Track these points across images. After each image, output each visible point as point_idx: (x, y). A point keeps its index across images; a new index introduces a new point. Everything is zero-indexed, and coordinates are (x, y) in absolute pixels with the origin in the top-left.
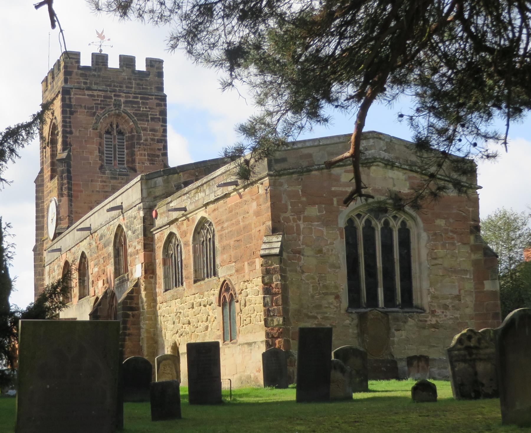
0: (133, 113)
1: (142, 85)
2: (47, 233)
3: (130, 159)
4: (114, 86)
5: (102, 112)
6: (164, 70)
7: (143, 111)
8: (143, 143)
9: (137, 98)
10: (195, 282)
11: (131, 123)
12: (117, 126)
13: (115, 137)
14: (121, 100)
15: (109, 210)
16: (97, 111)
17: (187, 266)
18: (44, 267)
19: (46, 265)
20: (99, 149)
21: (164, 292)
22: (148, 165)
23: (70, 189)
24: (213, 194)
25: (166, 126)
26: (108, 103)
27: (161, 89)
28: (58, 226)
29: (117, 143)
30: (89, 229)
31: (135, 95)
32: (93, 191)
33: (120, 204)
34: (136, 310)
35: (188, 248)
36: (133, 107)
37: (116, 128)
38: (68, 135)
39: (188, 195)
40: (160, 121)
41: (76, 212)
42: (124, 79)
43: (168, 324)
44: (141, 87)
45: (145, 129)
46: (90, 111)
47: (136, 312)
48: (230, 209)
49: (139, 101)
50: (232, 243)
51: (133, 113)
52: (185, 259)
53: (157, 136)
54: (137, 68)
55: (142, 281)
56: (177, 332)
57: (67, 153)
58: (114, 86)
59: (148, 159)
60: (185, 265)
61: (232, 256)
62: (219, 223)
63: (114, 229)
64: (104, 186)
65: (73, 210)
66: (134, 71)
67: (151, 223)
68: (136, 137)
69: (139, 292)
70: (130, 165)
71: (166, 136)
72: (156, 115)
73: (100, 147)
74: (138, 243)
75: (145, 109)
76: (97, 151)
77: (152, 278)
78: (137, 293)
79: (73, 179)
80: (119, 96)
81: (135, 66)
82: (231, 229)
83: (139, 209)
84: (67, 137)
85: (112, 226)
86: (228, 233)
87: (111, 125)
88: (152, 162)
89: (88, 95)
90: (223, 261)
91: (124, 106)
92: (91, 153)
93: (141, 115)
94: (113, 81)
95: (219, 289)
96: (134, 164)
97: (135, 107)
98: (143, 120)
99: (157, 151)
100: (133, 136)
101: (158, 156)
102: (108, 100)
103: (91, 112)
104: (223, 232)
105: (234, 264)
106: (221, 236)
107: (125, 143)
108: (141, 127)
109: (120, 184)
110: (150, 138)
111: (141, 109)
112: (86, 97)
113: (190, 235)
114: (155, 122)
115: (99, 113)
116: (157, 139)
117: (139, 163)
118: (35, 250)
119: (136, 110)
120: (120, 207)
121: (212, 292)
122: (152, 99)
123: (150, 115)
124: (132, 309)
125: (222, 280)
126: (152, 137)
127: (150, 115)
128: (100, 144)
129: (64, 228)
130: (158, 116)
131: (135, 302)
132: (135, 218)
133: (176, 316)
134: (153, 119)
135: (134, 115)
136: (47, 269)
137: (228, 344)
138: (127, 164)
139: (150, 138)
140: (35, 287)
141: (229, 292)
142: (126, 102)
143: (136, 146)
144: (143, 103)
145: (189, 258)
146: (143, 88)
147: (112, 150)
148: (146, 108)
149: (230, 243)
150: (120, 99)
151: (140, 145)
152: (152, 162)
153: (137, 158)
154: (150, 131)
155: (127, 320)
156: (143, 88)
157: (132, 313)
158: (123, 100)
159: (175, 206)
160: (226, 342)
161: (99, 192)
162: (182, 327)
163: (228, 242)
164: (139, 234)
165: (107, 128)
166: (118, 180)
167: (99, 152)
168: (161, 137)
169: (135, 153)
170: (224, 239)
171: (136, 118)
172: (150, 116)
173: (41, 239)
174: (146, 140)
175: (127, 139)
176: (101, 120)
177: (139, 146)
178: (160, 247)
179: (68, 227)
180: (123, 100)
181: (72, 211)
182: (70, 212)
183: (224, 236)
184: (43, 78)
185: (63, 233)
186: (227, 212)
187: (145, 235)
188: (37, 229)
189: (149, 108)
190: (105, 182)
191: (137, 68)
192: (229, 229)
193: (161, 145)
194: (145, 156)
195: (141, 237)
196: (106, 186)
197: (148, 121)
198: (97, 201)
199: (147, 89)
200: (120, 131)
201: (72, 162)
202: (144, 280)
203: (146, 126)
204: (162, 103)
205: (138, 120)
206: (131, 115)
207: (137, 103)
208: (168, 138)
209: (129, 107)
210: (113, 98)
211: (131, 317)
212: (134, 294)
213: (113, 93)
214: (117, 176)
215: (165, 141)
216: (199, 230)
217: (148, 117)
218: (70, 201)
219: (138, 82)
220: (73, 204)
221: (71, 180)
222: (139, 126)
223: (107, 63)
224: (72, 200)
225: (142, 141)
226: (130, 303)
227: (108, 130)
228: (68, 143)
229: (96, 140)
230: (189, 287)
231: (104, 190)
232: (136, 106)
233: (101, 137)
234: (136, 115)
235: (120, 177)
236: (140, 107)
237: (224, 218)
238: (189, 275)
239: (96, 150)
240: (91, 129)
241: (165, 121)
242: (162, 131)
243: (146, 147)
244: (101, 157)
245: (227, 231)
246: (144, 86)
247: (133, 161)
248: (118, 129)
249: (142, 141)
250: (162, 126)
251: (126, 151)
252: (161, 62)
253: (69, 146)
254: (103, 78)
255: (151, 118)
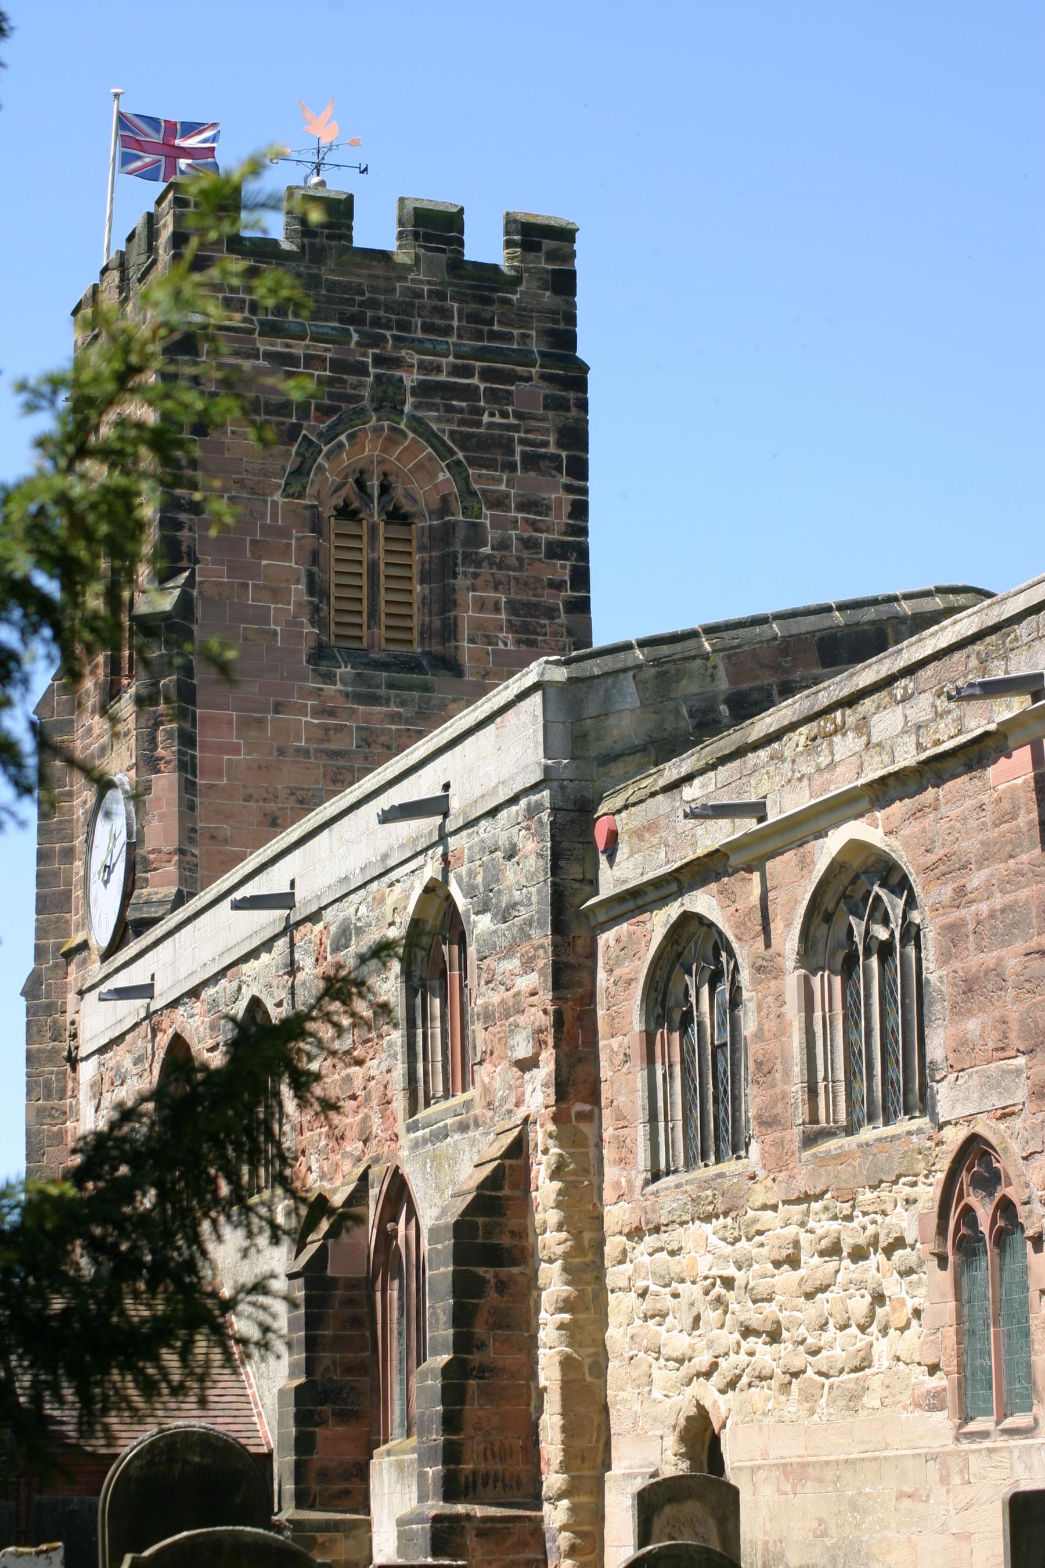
0: (452, 434)
1: (491, 323)
2: (86, 922)
3: (437, 623)
4: (376, 322)
5: (323, 426)
6: (580, 265)
7: (491, 425)
8: (488, 557)
9: (468, 372)
10: (810, 1140)
11: (444, 476)
12: (385, 489)
13: (373, 529)
14: (401, 379)
15: (390, 816)
16: (305, 423)
17: (765, 1068)
18: (73, 1061)
19: (83, 1053)
20: (311, 575)
21: (647, 1183)
22: (511, 647)
23: (187, 740)
24: (911, 740)
25: (585, 491)
26: (350, 391)
27: (569, 340)
28: (136, 892)
29: (382, 554)
30: (284, 900)
31: (459, 361)
32: (281, 752)
33: (439, 793)
34: (514, 1263)
35: (773, 984)
36: (450, 409)
37: (381, 495)
38: (183, 517)
39: (776, 745)
40: (559, 469)
41: (213, 837)
42: (419, 295)
43: (663, 1329)
44: (486, 328)
45: (499, 502)
46: (280, 419)
47: (515, 1270)
48: (1006, 805)
49: (477, 387)
50: (1012, 964)
51: (452, 434)
52: (759, 1035)
53: (548, 531)
54: (473, 252)
55: (539, 1136)
56: (714, 1366)
57: (177, 592)
58: (376, 322)
59: (509, 621)
60: (759, 1064)
61: (1014, 1025)
62: (942, 868)
63: (408, 897)
64: (326, 728)
65: (200, 825)
66: (458, 265)
67: (589, 876)
68: (461, 534)
69: (524, 1182)
70: (436, 648)
71: (584, 532)
72: (546, 444)
73: (315, 569)
74: (528, 966)
75: (498, 420)
76: (302, 587)
77: (581, 1116)
78: (515, 1186)
79: (199, 698)
80: (397, 363)
81: (461, 243)
82: (1009, 898)
83: (532, 812)
84: (179, 526)
85: (398, 887)
86: (992, 915)
87: (361, 484)
88: (523, 637)
89: (269, 356)
90: (961, 1046)
91: (417, 406)
92: (277, 594)
93: (484, 443)
94: (374, 304)
95: (941, 1176)
96: (453, 643)
97: (461, 411)
98: (491, 465)
99: (547, 591)
100: (450, 528)
101: (551, 612)
102: (352, 379)
103: (278, 424)
104: (967, 913)
105: (1021, 1061)
106: (953, 932)
107: (417, 557)
108: (484, 491)
109: (393, 723)
110: (520, 539)
111: (486, 419)
112: (261, 363)
113: (788, 925)
114: (539, 471)
115: (311, 429)
116: (550, 544)
117: (472, 641)
118: (31, 990)
119: (462, 422)
120: (438, 806)
121: (903, 1190)
122: (529, 379)
123: (523, 442)
124: (496, 1256)
125: (955, 1137)
126: (526, 535)
127: (523, 442)
128: (315, 558)
129: (161, 903)
130: (552, 449)
131: (513, 1223)
132: (509, 856)
133: (707, 1293)
134: (531, 461)
135: (453, 441)
136: (87, 1071)
137: (985, 1435)
138: (422, 642)
139: (520, 539)
140: (28, 1143)
141: (991, 1194)
142: (423, 389)
143: (460, 569)
144: (493, 396)
145: (782, 1031)
146: (494, 336)
147: (364, 582)
148: (504, 415)
149: (1000, 960)
150: (398, 373)
151: (479, 565)
152: (523, 637)
153: (467, 616)
154: (522, 507)
155: (476, 1306)
156: (494, 336)
157: (496, 1276)
158: (410, 379)
159: (707, 796)
160: (972, 1427)
161: (306, 753)
162: (738, 1344)
163: (989, 958)
164: (529, 922)
165: (343, 493)
166: (388, 705)
167: (311, 590)
168: (565, 534)
169: (459, 597)
170: (972, 947)
171: (460, 455)
172: (518, 449)
173: (59, 946)
174: (502, 545)
175: (426, 539)
176: (320, 460)
177: (471, 570)
178: (629, 982)
179: (180, 900)
180: (410, 379)
181: (194, 830)
182: (189, 834)
183: (971, 927)
184: (83, 291)
185: (160, 919)
186: (988, 818)
187: (559, 927)
188: (43, 905)
189: (518, 415)
190: (332, 713)
191: (473, 252)
192: (999, 901)
193: (563, 567)
194: (497, 610)
195: (542, 937)
196: (339, 729)
197: (511, 467)
198: (299, 793)
199: (508, 337)
200: (397, 508)
201: (195, 628)
202: (551, 1127)
203: (503, 487)
204: (572, 395)
205: (472, 462)
206: (444, 443)
207: (469, 393)
208: (595, 541)
209: (434, 407)
210: (371, 370)
211: (494, 1294)
212: (506, 1192)
213: (370, 351)
214: (383, 691)
215: (583, 553)
216: (831, 907)
217: (512, 453)
218: (188, 787)
219: (473, 306)
220: (198, 800)
221: (193, 701)
222: (476, 487)
223: (350, 228)
224: (194, 784)
225: (486, 550)
226: (489, 1232)
227: (347, 504)
228: (184, 549)
229: (299, 537)
230: (777, 1163)
231: (326, 746)
232: (464, 404)
233: (316, 526)
234: (462, 440)
235: (392, 692)
236: (480, 412)
237: (970, 846)
238: (779, 1109)
239: (298, 581)
240: (277, 497)
241: (579, 469)
242: (566, 509)
243: (500, 574)
244: (316, 609)
245: (984, 908)
246: (496, 328)
247: (449, 631)
248: (385, 498)
249: (486, 550)
250: (569, 489)
251: (418, 588)
252: (566, 235)
253: (184, 563)
254: (329, 290)
255: (523, 453)
